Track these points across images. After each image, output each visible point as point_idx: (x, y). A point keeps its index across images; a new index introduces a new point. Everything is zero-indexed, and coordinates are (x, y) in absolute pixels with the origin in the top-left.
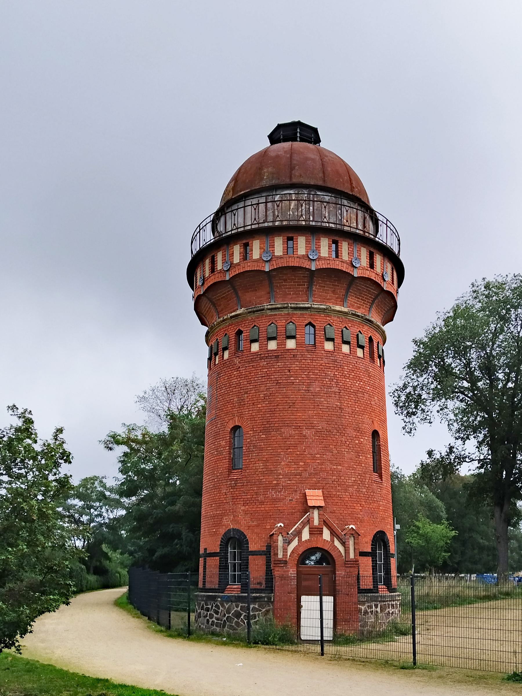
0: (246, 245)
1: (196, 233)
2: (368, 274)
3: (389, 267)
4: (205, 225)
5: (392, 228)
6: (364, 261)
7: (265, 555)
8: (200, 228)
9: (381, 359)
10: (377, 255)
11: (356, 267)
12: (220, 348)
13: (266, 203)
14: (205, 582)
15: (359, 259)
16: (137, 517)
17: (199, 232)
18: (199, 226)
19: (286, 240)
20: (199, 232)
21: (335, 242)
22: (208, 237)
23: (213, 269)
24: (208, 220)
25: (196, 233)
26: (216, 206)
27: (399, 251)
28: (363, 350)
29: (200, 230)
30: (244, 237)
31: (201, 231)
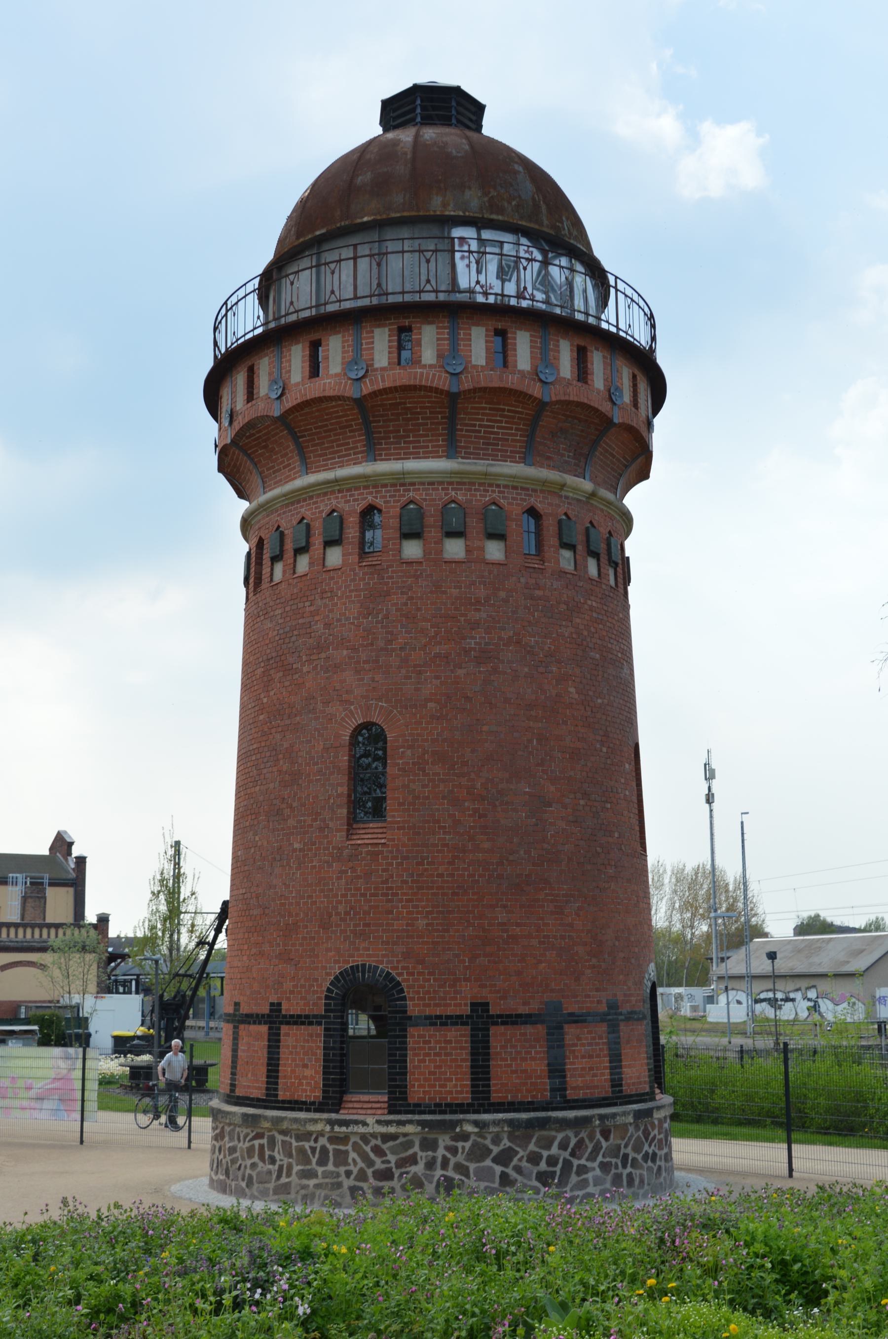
0: (315, 346)
1: (220, 318)
2: (576, 393)
3: (625, 373)
4: (236, 303)
5: (629, 292)
6: (566, 366)
7: (492, 1016)
8: (227, 308)
9: (619, 570)
10: (595, 352)
11: (551, 383)
12: (289, 546)
13: (355, 259)
14: (232, 1068)
15: (554, 366)
16: (754, 920)
17: (226, 315)
18: (226, 303)
19: (395, 332)
20: (226, 315)
21: (501, 333)
22: (248, 320)
23: (250, 396)
24: (250, 287)
25: (220, 318)
26: (266, 255)
27: (653, 338)
28: (575, 552)
29: (227, 311)
30: (311, 329)
31: (229, 313)
